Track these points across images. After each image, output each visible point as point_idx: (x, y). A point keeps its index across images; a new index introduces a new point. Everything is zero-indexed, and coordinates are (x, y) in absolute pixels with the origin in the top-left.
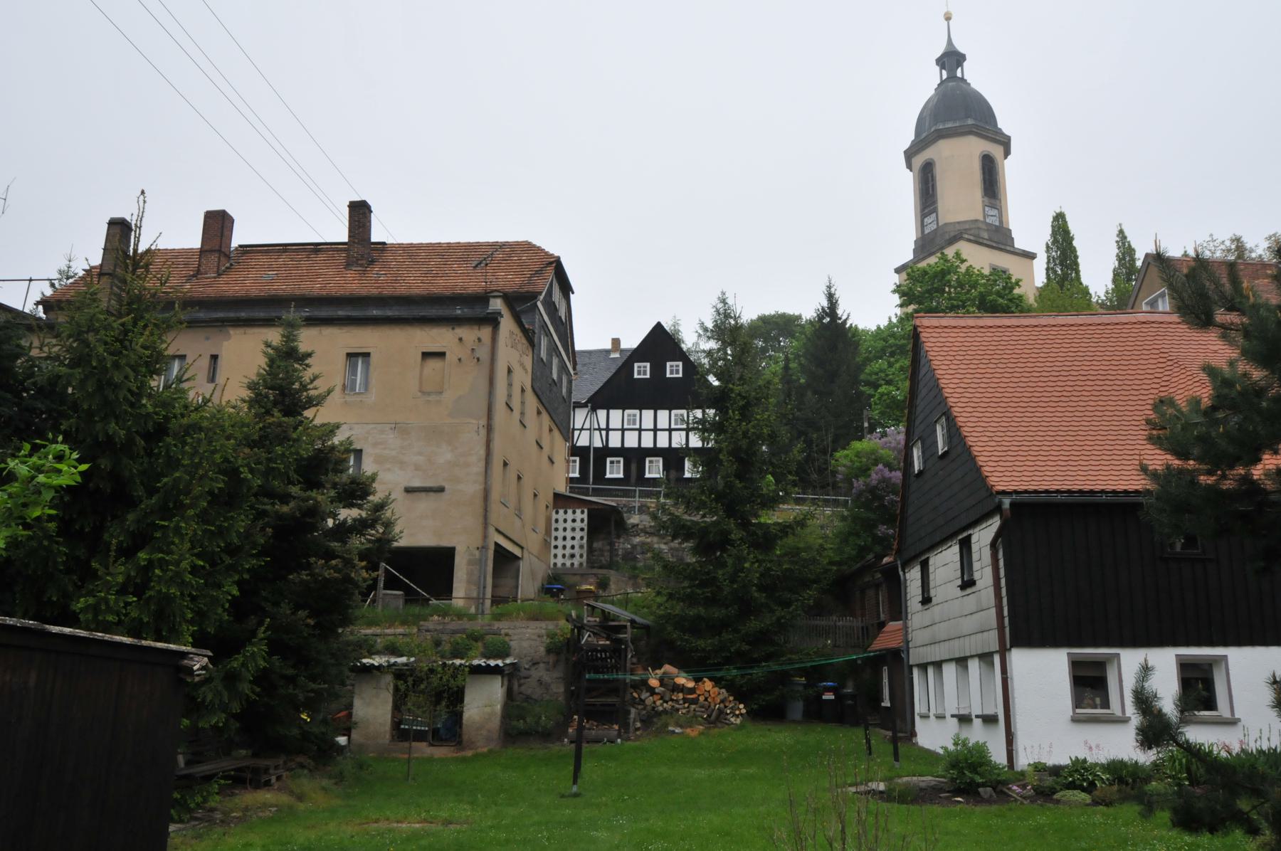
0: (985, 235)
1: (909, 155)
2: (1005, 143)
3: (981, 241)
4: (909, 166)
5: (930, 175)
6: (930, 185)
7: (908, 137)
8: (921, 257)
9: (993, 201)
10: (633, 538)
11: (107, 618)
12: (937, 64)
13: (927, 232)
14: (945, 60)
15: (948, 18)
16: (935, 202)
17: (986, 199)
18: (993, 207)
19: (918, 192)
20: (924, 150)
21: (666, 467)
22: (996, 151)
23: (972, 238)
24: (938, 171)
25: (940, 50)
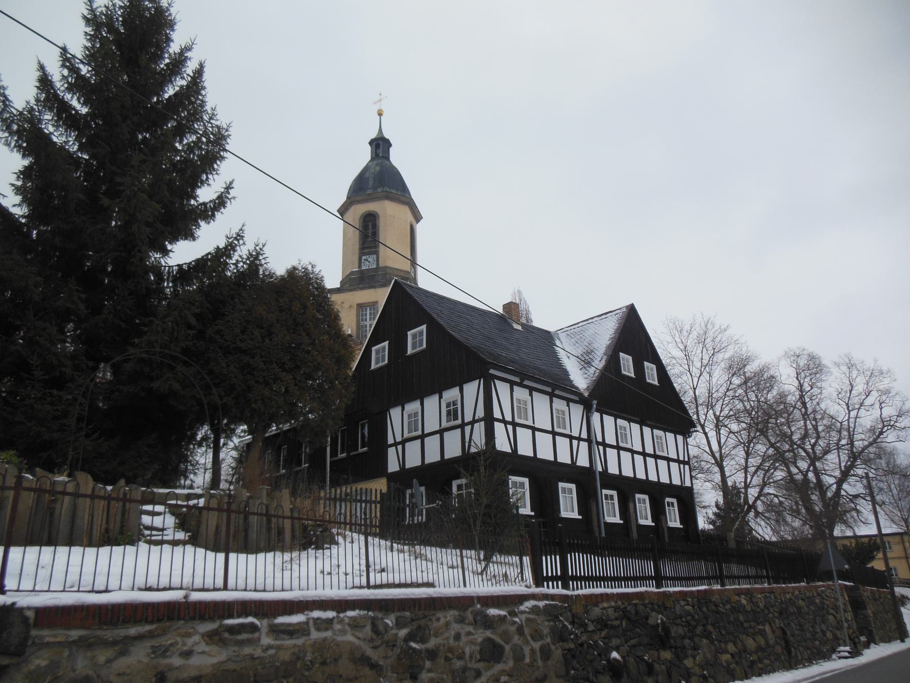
2: (418, 217)
5: (370, 224)
6: (370, 231)
15: (380, 114)
24: (382, 223)
25: (374, 135)
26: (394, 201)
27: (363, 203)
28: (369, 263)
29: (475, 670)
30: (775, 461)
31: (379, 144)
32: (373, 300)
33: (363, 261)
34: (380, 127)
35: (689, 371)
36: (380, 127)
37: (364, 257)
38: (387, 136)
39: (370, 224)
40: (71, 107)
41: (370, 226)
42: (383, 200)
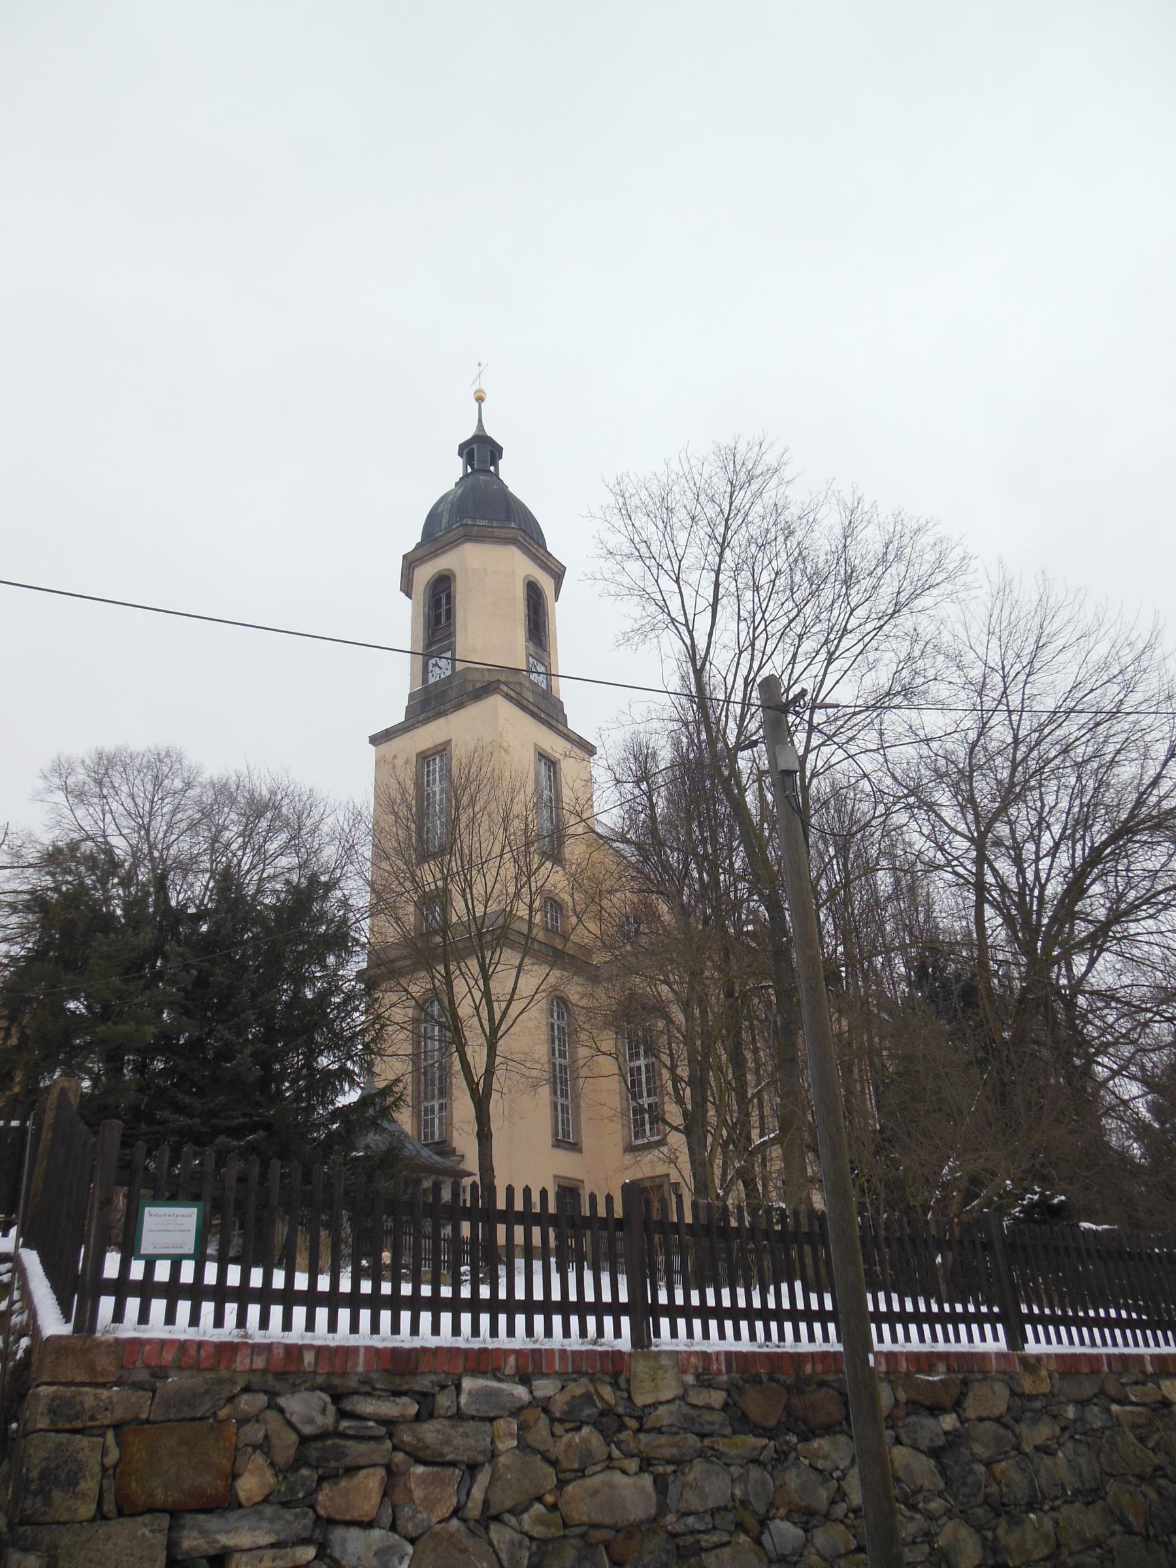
0: (530, 696)
1: (411, 563)
2: (557, 573)
3: (525, 702)
4: (407, 588)
5: (443, 596)
6: (443, 610)
7: (413, 537)
8: (421, 717)
9: (540, 652)
10: (663, 994)
11: (388, 1262)
12: (461, 454)
13: (431, 680)
14: (475, 446)
15: (480, 400)
16: (451, 634)
17: (531, 645)
18: (540, 661)
19: (421, 621)
20: (436, 556)
21: (259, 1354)
22: (546, 583)
23: (513, 694)
24: (460, 589)
25: (468, 433)
26: (484, 542)
27: (431, 559)
28: (441, 670)
29: (561, 1437)
30: (816, 728)
31: (473, 450)
32: (440, 739)
33: (430, 668)
34: (480, 421)
35: (687, 625)
36: (480, 421)
37: (433, 661)
38: (490, 432)
39: (443, 596)
40: (250, 1133)
41: (444, 601)
42: (461, 543)
